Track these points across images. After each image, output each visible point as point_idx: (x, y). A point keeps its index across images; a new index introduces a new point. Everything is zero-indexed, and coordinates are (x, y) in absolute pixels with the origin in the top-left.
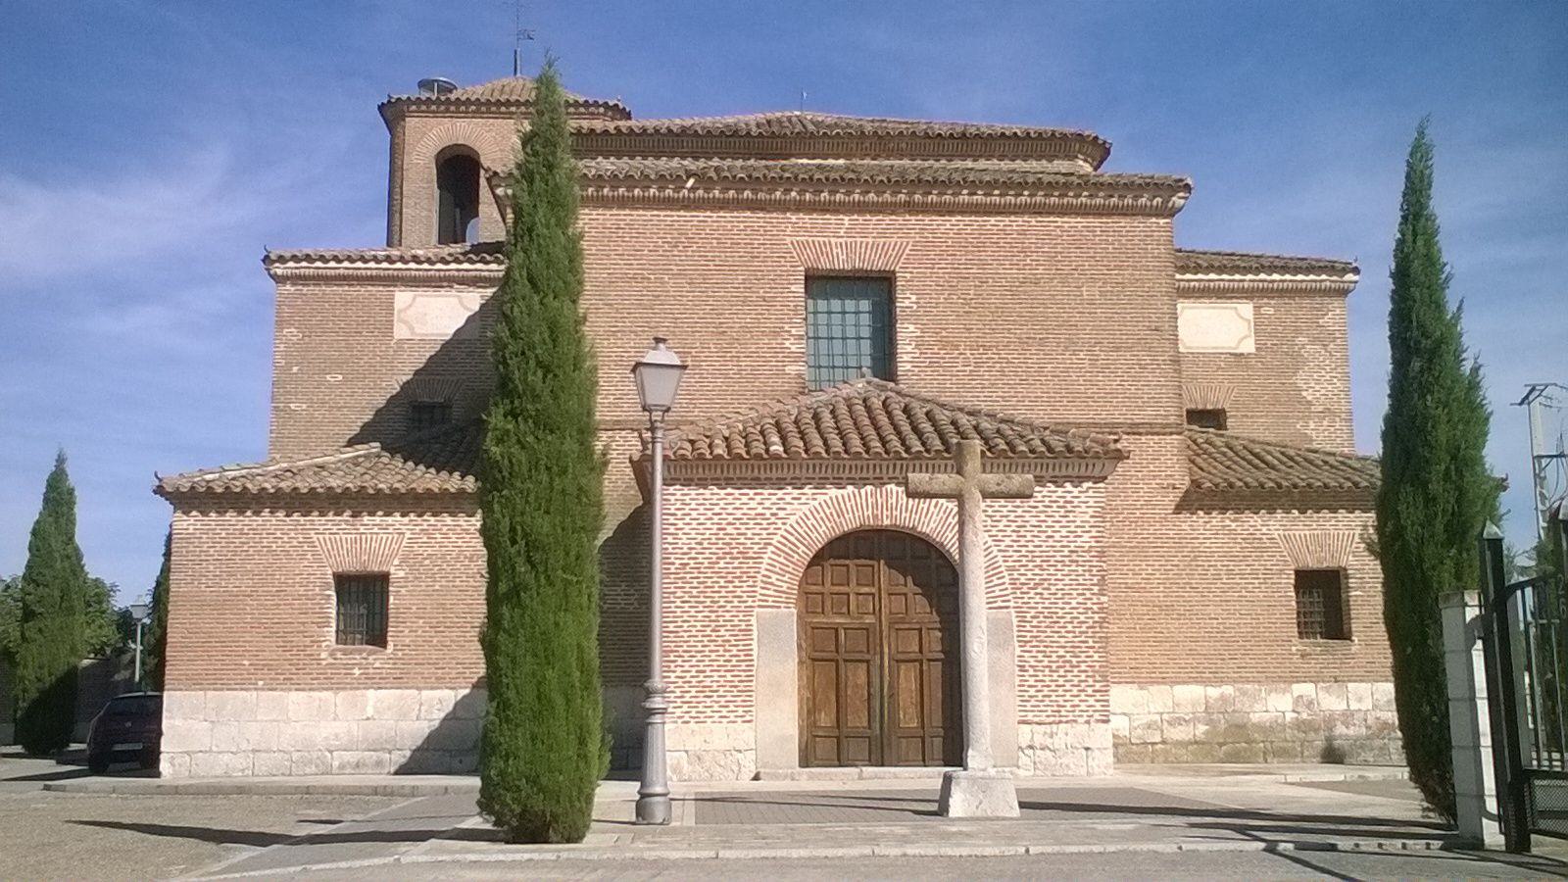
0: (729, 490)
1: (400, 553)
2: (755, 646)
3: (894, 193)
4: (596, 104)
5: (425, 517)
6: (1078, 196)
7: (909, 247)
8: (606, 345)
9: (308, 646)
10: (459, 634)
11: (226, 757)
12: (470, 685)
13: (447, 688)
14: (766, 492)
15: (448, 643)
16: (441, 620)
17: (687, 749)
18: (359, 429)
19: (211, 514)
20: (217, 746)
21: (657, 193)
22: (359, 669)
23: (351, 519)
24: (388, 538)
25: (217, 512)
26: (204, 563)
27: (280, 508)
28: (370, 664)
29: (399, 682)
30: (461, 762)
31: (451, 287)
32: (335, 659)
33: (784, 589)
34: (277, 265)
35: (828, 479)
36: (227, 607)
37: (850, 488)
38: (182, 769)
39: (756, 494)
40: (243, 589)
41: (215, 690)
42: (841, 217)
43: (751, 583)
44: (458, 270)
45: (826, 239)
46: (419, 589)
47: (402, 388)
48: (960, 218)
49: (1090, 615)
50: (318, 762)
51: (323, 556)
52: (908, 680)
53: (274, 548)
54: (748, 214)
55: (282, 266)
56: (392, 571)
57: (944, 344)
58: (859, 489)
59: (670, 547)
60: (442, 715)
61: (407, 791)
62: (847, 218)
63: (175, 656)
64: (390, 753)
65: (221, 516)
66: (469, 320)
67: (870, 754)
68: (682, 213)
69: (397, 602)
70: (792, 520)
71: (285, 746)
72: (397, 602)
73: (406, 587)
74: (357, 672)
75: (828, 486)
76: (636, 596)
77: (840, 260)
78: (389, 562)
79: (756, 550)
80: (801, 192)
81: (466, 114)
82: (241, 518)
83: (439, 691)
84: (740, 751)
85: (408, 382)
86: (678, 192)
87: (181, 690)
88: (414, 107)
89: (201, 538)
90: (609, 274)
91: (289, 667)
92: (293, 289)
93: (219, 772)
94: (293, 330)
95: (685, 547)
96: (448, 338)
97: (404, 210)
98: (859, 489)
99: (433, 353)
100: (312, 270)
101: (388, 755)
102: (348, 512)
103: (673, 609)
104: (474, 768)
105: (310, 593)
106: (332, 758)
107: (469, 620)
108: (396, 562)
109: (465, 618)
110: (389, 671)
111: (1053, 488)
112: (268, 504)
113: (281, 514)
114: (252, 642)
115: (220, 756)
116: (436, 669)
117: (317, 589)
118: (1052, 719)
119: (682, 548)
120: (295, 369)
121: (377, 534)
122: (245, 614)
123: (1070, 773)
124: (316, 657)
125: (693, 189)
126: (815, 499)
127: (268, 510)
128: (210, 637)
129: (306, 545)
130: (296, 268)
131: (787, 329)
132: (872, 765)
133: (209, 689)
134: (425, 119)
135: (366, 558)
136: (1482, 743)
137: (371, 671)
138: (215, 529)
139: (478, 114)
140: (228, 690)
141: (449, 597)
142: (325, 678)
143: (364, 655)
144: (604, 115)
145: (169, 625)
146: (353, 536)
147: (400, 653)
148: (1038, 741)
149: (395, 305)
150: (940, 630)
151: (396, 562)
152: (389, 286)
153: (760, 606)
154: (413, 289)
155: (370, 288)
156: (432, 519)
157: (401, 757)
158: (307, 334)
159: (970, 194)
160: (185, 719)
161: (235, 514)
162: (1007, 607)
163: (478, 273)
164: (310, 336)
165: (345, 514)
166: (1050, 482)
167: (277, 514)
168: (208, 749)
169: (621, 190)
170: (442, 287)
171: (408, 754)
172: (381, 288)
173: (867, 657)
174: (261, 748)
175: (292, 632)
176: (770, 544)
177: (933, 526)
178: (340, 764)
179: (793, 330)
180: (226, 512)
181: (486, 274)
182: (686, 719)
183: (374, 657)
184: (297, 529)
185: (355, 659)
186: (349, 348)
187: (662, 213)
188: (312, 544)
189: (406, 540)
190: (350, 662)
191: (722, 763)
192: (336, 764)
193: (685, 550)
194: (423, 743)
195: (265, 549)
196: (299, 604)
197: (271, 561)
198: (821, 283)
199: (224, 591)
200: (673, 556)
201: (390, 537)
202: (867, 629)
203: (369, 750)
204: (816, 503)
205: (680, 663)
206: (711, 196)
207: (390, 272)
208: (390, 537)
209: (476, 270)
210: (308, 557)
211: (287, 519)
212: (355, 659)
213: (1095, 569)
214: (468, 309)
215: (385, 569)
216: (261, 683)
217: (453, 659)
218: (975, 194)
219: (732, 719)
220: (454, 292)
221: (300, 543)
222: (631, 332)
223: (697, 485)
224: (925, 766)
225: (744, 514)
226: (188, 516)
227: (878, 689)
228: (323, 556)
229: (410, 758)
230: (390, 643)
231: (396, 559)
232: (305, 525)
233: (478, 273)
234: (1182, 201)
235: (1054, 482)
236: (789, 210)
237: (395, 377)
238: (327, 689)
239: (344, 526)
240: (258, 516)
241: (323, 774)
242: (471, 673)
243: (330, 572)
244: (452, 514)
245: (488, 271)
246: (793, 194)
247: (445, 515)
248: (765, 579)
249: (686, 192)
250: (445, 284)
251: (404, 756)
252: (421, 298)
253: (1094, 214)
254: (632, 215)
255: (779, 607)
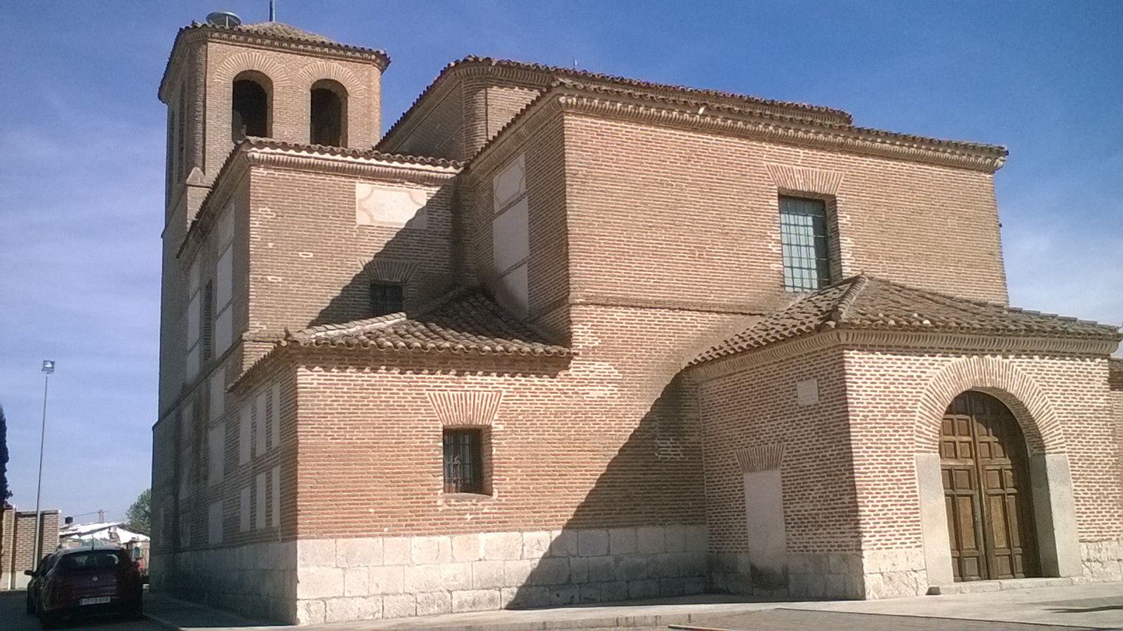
0: (889, 356)
1: (499, 409)
2: (917, 485)
3: (836, 136)
4: (370, 52)
5: (517, 378)
6: (945, 152)
7: (843, 178)
8: (645, 237)
9: (426, 494)
10: (550, 481)
11: (358, 601)
12: (561, 527)
13: (543, 529)
14: (912, 358)
15: (542, 490)
16: (535, 468)
17: (882, 571)
18: (329, 302)
19: (333, 370)
20: (350, 592)
21: (678, 116)
22: (470, 514)
23: (456, 377)
24: (488, 395)
25: (339, 368)
26: (329, 416)
27: (395, 366)
28: (479, 510)
29: (503, 525)
30: (558, 596)
31: (403, 183)
32: (450, 505)
33: (931, 437)
34: (254, 149)
35: (952, 349)
36: (353, 458)
37: (964, 356)
38: (318, 616)
39: (906, 359)
40: (366, 440)
41: (343, 537)
42: (798, 150)
43: (909, 433)
44: (411, 169)
45: (790, 166)
46: (516, 441)
47: (364, 268)
48: (871, 160)
49: (1110, 458)
50: (440, 602)
51: (435, 411)
52: (996, 511)
53: (391, 403)
54: (737, 140)
55: (259, 151)
56: (493, 425)
57: (870, 255)
58: (970, 358)
59: (855, 401)
60: (541, 554)
61: (650, 621)
62: (801, 151)
63: (306, 506)
64: (500, 590)
65: (343, 371)
66: (419, 213)
67: (979, 570)
68: (691, 134)
69: (498, 453)
70: (931, 381)
71: (413, 591)
72: (498, 453)
73: (506, 439)
74: (468, 517)
75: (951, 355)
76: (681, 448)
77: (799, 184)
78: (490, 418)
79: (910, 405)
80: (776, 127)
81: (260, 47)
82: (360, 374)
83: (538, 532)
84: (915, 571)
85: (370, 263)
86: (693, 117)
87: (313, 538)
88: (216, 35)
89: (325, 392)
90: (643, 178)
91: (410, 514)
92: (266, 172)
93: (353, 616)
94: (267, 209)
95: (865, 401)
96: (402, 227)
97: (207, 121)
98: (970, 358)
99: (390, 239)
100: (286, 157)
101: (498, 592)
102: (453, 372)
103: (862, 454)
104: (569, 600)
105: (425, 445)
106: (452, 598)
107: (557, 468)
108: (496, 417)
109: (554, 467)
110: (495, 515)
111: (1080, 362)
112: (386, 362)
113: (396, 371)
114: (376, 490)
115: (353, 601)
116: (534, 512)
117: (431, 440)
118: (1098, 538)
119: (862, 403)
120: (270, 245)
121: (479, 391)
122: (368, 464)
123: (1113, 579)
124: (433, 504)
125: (703, 116)
126: (943, 365)
127: (384, 367)
128: (336, 487)
129: (419, 400)
130: (272, 154)
131: (769, 234)
132: (982, 579)
133: (339, 537)
134: (224, 46)
135: (471, 413)
136: (98, 599)
137: (481, 516)
138: (338, 384)
139: (271, 47)
140: (356, 537)
141: (539, 449)
142: (441, 524)
143: (474, 501)
144: (374, 61)
145: (299, 476)
146: (459, 393)
147: (504, 499)
148: (1093, 554)
149: (357, 195)
150: (1011, 470)
151: (496, 417)
152: (351, 177)
153: (917, 451)
154: (371, 182)
155: (334, 178)
156: (523, 379)
157: (509, 594)
158: (280, 214)
159: (882, 142)
160: (319, 566)
161: (355, 370)
162: (1063, 452)
163: (427, 173)
164: (282, 216)
165: (451, 373)
166: (1078, 357)
167: (393, 371)
168: (341, 595)
169: (652, 110)
170: (396, 182)
171: (515, 590)
172: (343, 179)
173: (971, 492)
174: (389, 592)
175: (412, 481)
176: (919, 401)
177: (1015, 388)
178: (459, 602)
179: (773, 235)
180: (347, 368)
181: (434, 174)
182: (879, 546)
183: (483, 503)
184: (411, 386)
185: (467, 505)
186: (317, 228)
187: (678, 133)
188: (424, 400)
189: (502, 398)
190: (463, 508)
191: (906, 582)
192: (455, 603)
193: (865, 405)
194: (528, 580)
195: (383, 404)
196: (416, 455)
197: (389, 415)
198: (791, 200)
199: (348, 443)
200: (858, 409)
201: (490, 394)
202: (969, 470)
203: (483, 589)
204: (944, 368)
205: (870, 499)
206: (715, 122)
207: (355, 165)
208: (490, 394)
209: (426, 170)
210: (422, 411)
211: (402, 376)
212: (467, 505)
213: (1109, 423)
214: (418, 204)
215: (487, 423)
216: (386, 529)
217: (547, 503)
218: (885, 143)
219: (909, 545)
220: (404, 188)
221: (413, 398)
222: (662, 227)
223: (868, 350)
224: (1015, 578)
225: (900, 376)
226: (311, 371)
227: (980, 517)
228: (435, 411)
229: (518, 594)
230: (495, 490)
231: (496, 415)
232: (418, 382)
233: (427, 173)
234: (1002, 163)
235: (1080, 357)
236: (764, 140)
237: (358, 257)
238: (444, 534)
239: (450, 384)
240: (374, 372)
241: (444, 613)
242: (561, 516)
243: (441, 426)
244: (539, 375)
245: (436, 172)
246: (771, 128)
247: (533, 376)
248: (918, 429)
249: (698, 117)
250: (398, 180)
251: (512, 593)
252: (380, 191)
253: (914, 161)
254: (656, 132)
255: (929, 452)
